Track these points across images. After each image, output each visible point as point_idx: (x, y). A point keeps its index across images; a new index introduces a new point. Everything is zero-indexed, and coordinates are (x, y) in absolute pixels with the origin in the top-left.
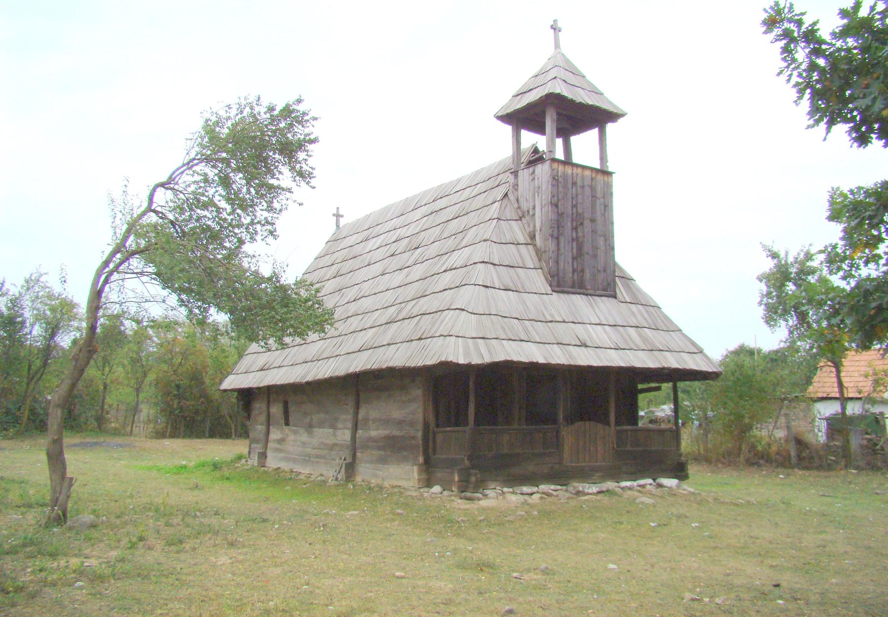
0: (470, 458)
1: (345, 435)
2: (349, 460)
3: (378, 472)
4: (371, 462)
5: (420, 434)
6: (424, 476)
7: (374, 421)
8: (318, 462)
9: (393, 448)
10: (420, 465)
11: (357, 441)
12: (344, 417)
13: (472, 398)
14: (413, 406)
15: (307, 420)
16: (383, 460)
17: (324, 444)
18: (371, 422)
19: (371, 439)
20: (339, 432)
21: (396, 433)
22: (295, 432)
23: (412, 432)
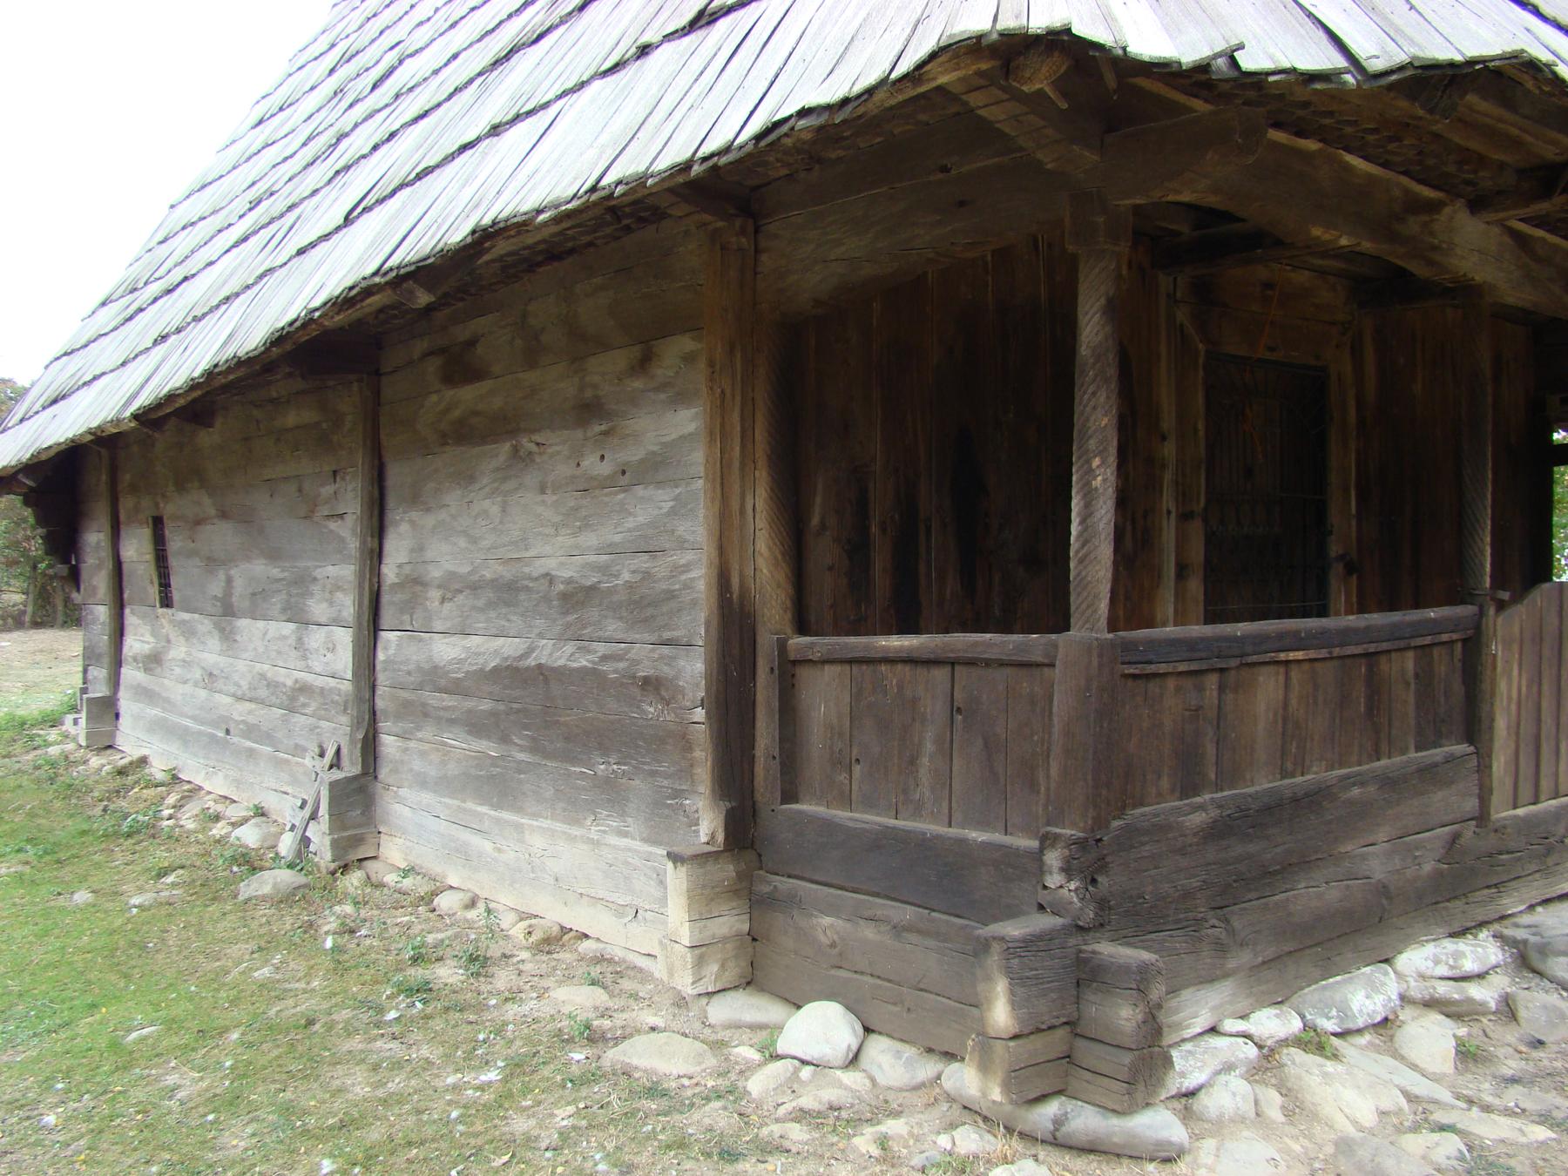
0: (1088, 863)
1: (333, 652)
2: (351, 768)
3: (476, 841)
4: (444, 785)
5: (693, 670)
6: (730, 922)
7: (453, 587)
8: (251, 753)
9: (549, 727)
10: (701, 858)
11: (382, 678)
12: (331, 570)
13: (1097, 416)
14: (647, 507)
15: (216, 587)
16: (496, 787)
17: (273, 685)
18: (435, 594)
19: (434, 678)
20: (316, 638)
21: (556, 654)
22: (189, 632)
23: (645, 657)
